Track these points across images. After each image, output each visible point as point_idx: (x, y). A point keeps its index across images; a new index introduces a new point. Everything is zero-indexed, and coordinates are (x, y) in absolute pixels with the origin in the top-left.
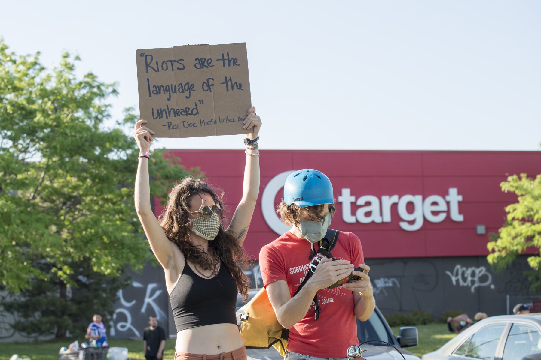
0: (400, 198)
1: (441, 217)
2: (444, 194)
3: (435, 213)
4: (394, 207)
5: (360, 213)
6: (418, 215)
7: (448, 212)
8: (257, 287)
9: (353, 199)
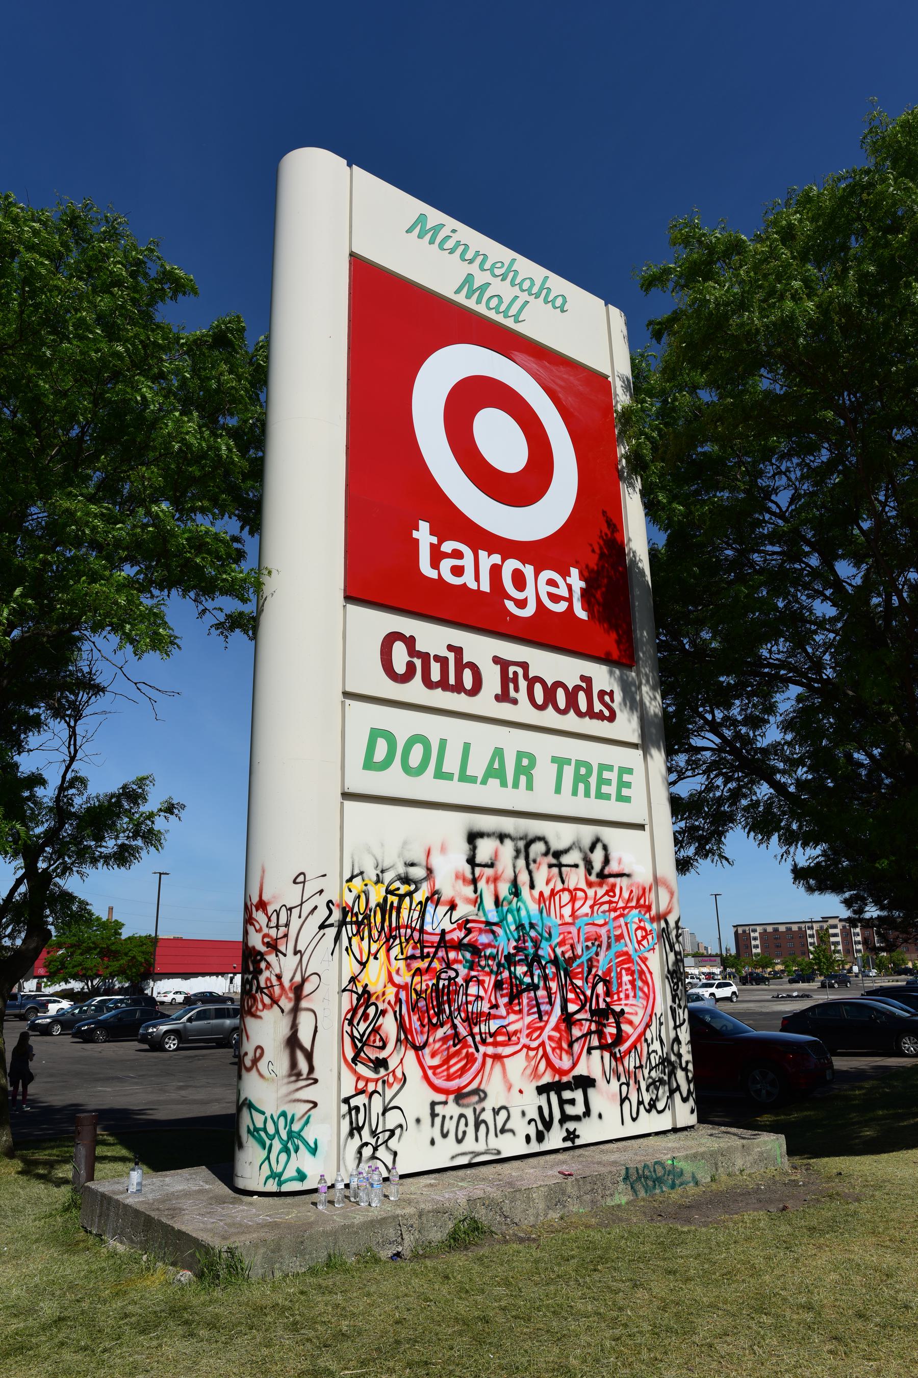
0: (503, 561)
1: (562, 607)
2: (565, 574)
3: (555, 598)
4: (496, 571)
5: (446, 565)
6: (529, 593)
7: (570, 600)
8: (573, 763)
9: (435, 540)
